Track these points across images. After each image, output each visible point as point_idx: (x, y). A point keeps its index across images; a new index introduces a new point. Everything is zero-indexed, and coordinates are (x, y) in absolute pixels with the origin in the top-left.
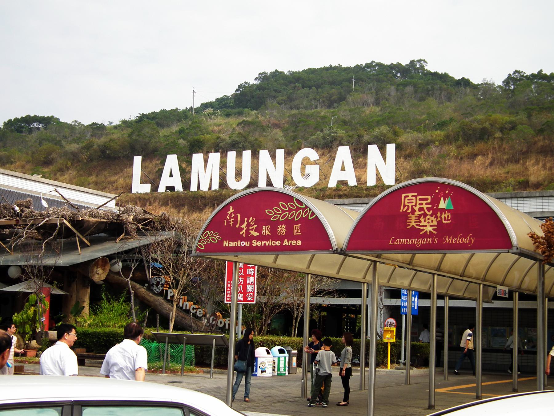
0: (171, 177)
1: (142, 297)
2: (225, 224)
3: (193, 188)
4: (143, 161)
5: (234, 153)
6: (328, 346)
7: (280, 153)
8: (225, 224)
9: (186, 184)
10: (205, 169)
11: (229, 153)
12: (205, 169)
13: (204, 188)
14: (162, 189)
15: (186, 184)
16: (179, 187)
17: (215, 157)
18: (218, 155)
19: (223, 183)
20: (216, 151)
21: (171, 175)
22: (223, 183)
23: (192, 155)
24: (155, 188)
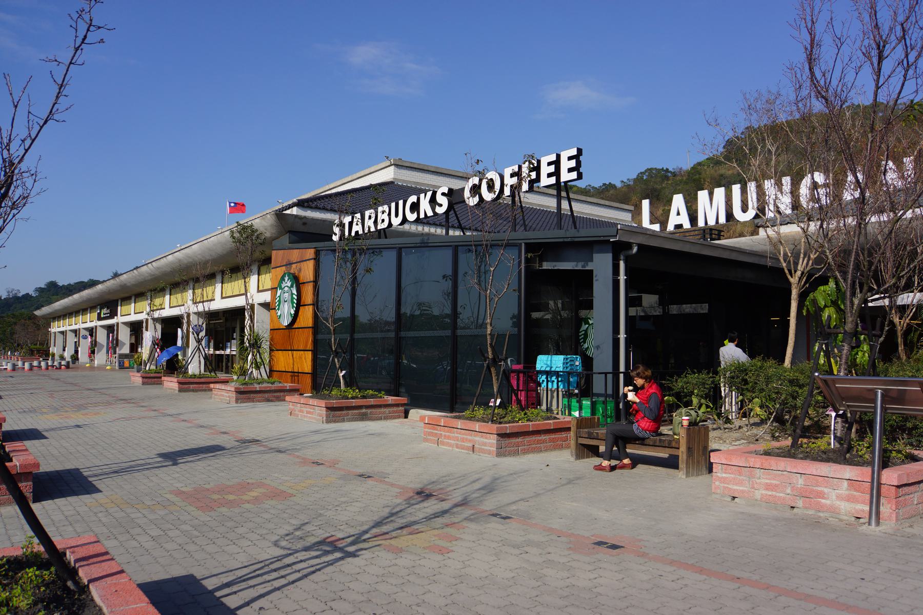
0: (678, 216)
1: (639, 179)
2: (704, 308)
3: (701, 223)
4: (651, 203)
5: (738, 186)
6: (647, 366)
7: (786, 181)
8: (704, 308)
9: (693, 219)
10: (711, 204)
11: (734, 186)
12: (711, 204)
13: (711, 222)
14: (670, 227)
15: (693, 219)
16: (687, 225)
17: (720, 192)
18: (723, 189)
19: (730, 216)
20: (720, 186)
21: (678, 214)
22: (730, 216)
23: (696, 195)
24: (664, 224)
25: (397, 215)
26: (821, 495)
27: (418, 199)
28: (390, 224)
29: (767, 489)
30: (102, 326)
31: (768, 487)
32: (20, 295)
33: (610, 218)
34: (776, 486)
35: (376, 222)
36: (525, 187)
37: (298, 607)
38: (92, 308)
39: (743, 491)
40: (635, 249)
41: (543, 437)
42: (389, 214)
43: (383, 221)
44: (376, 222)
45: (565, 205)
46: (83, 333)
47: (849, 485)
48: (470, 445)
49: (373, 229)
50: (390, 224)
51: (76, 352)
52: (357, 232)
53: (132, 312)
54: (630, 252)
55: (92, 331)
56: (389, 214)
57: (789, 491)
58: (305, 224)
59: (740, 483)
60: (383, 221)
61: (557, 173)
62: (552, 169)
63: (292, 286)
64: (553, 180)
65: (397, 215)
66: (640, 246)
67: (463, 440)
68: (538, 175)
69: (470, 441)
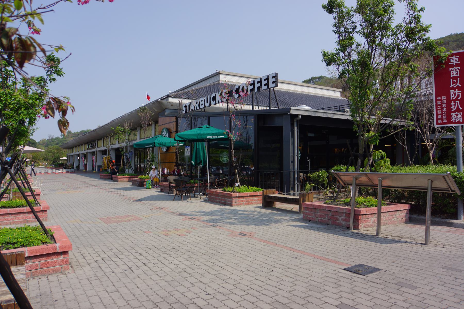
25: (207, 102)
26: (337, 219)
27: (216, 95)
28: (205, 106)
29: (320, 217)
30: (90, 153)
31: (321, 216)
32: (54, 138)
33: (330, 96)
34: (323, 216)
35: (199, 105)
36: (256, 90)
37: (230, 293)
38: (85, 144)
39: (312, 218)
40: (300, 116)
41: (254, 198)
42: (204, 102)
43: (202, 104)
44: (199, 105)
45: (230, 106)
46: (81, 156)
47: (346, 215)
48: (224, 202)
49: (198, 108)
50: (205, 106)
51: (79, 164)
52: (192, 110)
53: (117, 143)
54: (298, 119)
55: (85, 156)
56: (204, 102)
57: (327, 218)
58: (172, 105)
59: (312, 215)
60: (202, 104)
61: (267, 84)
62: (266, 82)
63: (166, 134)
64: (266, 87)
65: (207, 102)
66: (302, 115)
67: (222, 200)
68: (261, 85)
69: (224, 200)
